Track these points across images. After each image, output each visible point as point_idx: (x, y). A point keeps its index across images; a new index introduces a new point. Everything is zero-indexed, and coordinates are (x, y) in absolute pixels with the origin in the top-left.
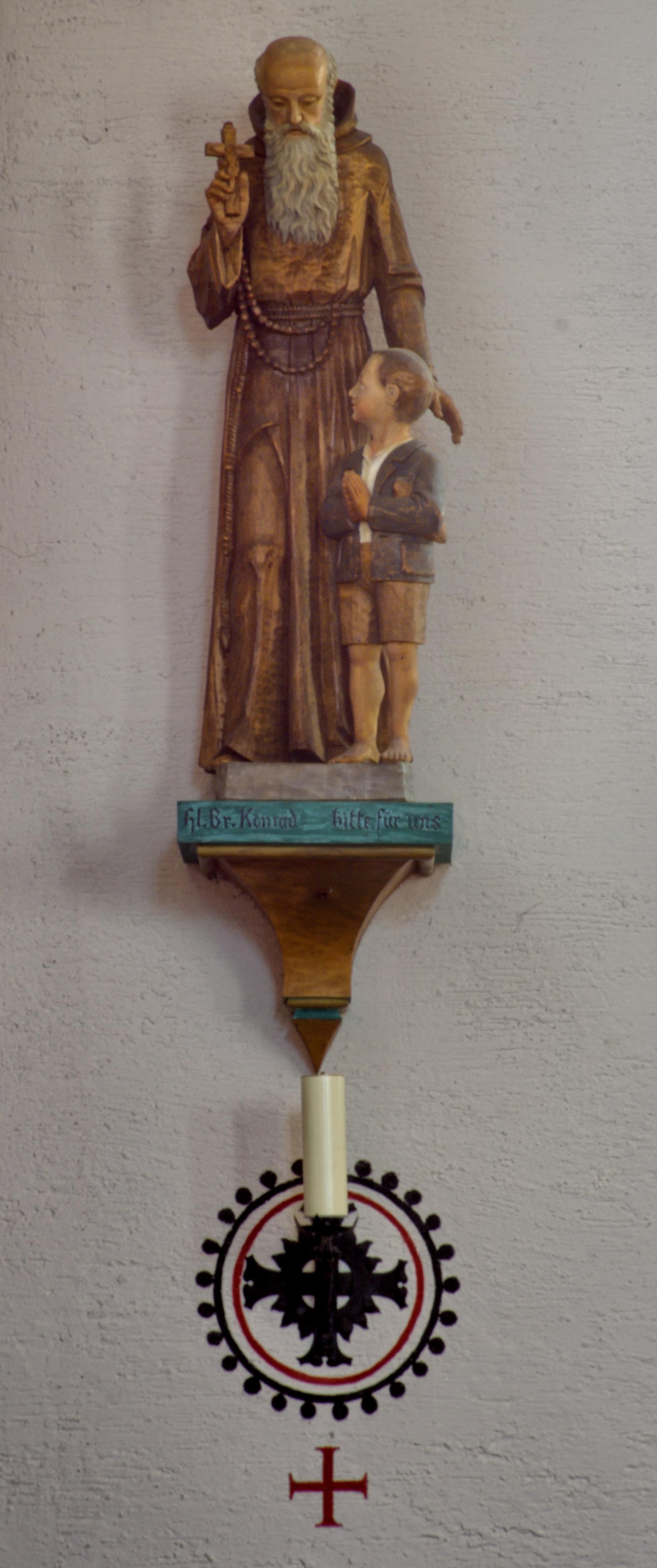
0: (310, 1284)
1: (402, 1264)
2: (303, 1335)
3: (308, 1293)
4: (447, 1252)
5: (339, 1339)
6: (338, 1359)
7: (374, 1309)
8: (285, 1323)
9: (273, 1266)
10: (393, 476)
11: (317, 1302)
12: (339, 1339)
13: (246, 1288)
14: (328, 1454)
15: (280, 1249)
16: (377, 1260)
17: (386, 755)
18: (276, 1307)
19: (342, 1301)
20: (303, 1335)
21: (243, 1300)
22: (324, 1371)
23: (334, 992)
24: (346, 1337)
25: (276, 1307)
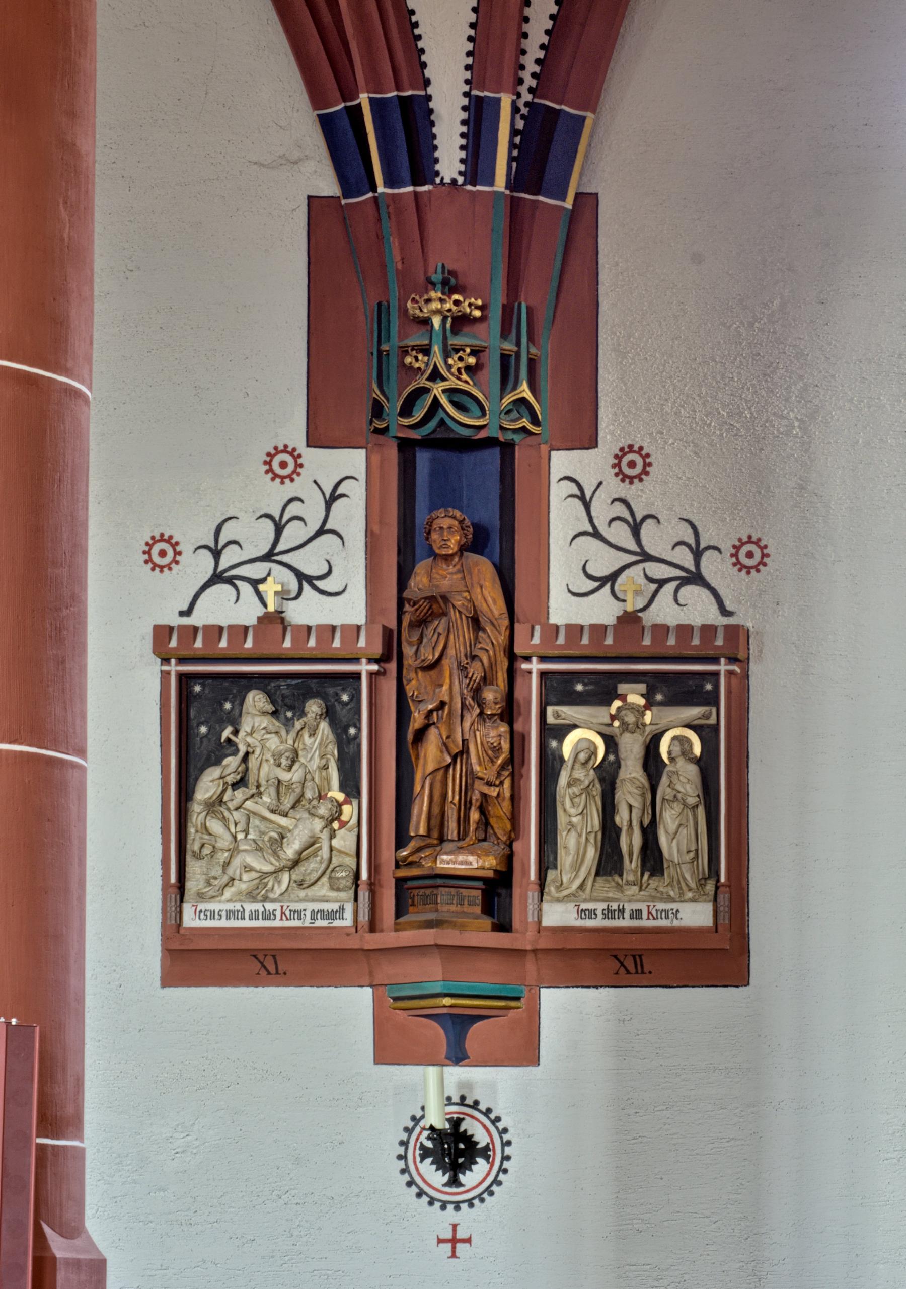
0: (460, 1153)
1: (422, 1161)
6: (423, 1158)
19: (461, 1160)
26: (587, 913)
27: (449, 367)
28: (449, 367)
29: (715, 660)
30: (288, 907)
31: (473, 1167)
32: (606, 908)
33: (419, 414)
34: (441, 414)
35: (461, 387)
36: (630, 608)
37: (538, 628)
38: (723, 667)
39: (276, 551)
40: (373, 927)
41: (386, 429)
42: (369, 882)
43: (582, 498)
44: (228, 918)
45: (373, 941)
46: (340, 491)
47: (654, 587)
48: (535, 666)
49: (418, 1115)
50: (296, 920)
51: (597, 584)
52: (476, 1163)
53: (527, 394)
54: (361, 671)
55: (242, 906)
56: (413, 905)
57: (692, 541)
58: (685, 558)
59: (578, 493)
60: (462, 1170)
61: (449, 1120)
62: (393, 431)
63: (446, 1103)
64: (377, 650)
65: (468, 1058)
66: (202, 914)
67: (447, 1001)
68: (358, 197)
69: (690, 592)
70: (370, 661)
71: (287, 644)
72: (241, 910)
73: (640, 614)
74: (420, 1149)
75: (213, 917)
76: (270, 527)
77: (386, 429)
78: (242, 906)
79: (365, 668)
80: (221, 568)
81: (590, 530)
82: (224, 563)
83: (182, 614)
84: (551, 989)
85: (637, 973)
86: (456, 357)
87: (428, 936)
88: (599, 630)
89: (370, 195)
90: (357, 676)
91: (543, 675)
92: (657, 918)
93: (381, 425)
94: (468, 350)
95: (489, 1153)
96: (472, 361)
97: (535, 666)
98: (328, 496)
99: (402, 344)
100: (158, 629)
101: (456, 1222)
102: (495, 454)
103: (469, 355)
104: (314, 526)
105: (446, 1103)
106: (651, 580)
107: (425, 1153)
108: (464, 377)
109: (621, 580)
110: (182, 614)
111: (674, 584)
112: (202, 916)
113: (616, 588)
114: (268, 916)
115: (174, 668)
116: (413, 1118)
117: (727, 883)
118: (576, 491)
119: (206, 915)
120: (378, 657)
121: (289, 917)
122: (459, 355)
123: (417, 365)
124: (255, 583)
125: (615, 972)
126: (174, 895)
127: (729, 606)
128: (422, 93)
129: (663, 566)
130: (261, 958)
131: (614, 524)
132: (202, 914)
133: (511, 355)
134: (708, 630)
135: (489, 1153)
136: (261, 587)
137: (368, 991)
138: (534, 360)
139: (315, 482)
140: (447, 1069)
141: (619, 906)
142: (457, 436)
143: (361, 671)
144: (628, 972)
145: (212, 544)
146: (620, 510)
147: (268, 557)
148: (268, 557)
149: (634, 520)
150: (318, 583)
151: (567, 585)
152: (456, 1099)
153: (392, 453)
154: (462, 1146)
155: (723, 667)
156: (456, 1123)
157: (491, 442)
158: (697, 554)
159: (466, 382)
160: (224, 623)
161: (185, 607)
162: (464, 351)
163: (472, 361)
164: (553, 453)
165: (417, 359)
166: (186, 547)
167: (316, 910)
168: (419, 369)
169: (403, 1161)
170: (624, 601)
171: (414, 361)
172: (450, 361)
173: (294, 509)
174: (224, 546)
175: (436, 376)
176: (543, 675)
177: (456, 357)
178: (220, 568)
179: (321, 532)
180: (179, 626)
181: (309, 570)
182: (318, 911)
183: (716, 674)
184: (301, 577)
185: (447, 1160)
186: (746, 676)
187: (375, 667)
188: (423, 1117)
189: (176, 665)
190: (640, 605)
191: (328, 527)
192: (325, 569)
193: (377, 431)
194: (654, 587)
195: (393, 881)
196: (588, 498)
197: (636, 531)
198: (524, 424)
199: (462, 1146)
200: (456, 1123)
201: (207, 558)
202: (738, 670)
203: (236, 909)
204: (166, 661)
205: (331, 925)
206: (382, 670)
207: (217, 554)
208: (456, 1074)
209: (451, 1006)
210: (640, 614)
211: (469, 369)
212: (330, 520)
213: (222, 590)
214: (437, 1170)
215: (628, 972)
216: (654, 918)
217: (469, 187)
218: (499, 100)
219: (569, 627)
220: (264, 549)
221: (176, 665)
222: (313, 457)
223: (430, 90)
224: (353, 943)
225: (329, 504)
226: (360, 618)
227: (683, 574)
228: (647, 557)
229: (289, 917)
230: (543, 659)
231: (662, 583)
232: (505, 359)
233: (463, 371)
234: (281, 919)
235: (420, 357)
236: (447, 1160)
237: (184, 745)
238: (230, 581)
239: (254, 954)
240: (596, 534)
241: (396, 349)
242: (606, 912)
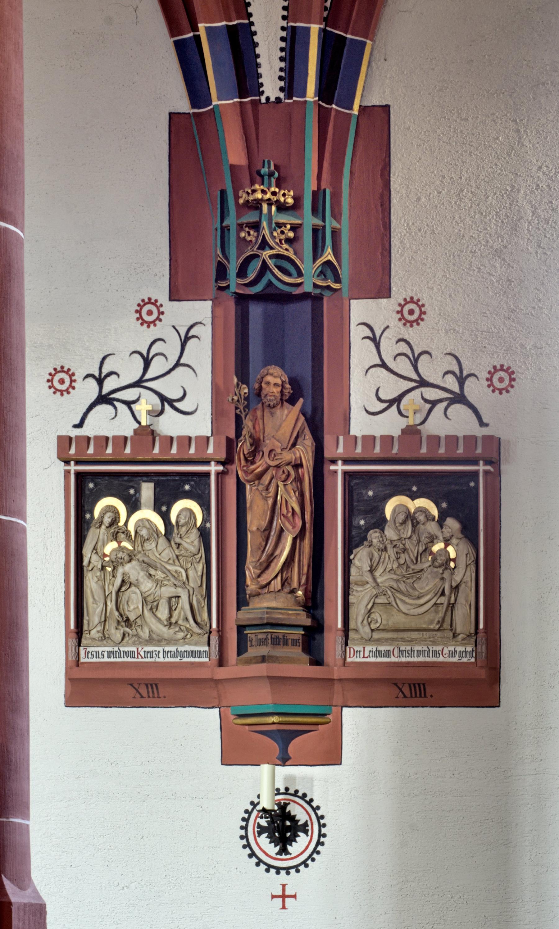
0: (289, 829)
1: (307, 821)
2: (289, 812)
13: (258, 831)
14: (284, 886)
16: (267, 837)
18: (267, 837)
19: (288, 834)
21: (257, 835)
22: (284, 857)
23: (300, 222)
25: (267, 837)
27: (274, 238)
28: (274, 238)
29: (475, 462)
31: (273, 844)
33: (251, 276)
34: (268, 276)
35: (282, 253)
36: (411, 423)
37: (341, 438)
38: (481, 468)
40: (221, 662)
41: (228, 287)
42: (217, 629)
43: (373, 339)
44: (109, 657)
45: (222, 673)
46: (190, 334)
47: (428, 406)
48: (340, 467)
49: (256, 801)
51: (385, 405)
52: (299, 836)
53: (331, 258)
54: (211, 471)
55: (119, 649)
56: (252, 646)
57: (457, 371)
58: (452, 383)
60: (288, 842)
61: (279, 804)
62: (233, 289)
63: (276, 792)
64: (223, 456)
66: (90, 654)
67: (275, 719)
68: (204, 108)
69: (458, 409)
70: (218, 463)
71: (156, 450)
72: (428, 650)
73: (419, 427)
74: (258, 828)
76: (140, 363)
77: (228, 287)
78: (119, 649)
79: (213, 468)
80: (105, 391)
83: (75, 426)
85: (412, 697)
86: (279, 231)
87: (262, 669)
88: (388, 440)
90: (207, 475)
91: (346, 474)
93: (224, 284)
94: (289, 227)
95: (307, 828)
96: (291, 235)
97: (340, 467)
99: (240, 221)
100: (60, 439)
102: (307, 306)
103: (289, 230)
104: (172, 362)
105: (276, 792)
106: (426, 401)
107: (261, 830)
108: (285, 246)
109: (404, 402)
110: (75, 426)
111: (445, 404)
112: (90, 656)
113: (402, 407)
114: (435, 653)
115: (73, 468)
116: (252, 803)
118: (369, 334)
120: (223, 460)
122: (282, 229)
123: (249, 238)
124: (129, 404)
125: (396, 696)
126: (73, 642)
127: (485, 420)
128: (247, 21)
130: (136, 686)
131: (399, 358)
132: (90, 654)
133: (319, 229)
134: (470, 440)
136: (135, 407)
138: (336, 232)
140: (277, 768)
142: (277, 292)
143: (211, 471)
144: (405, 696)
146: (403, 348)
147: (137, 384)
148: (137, 384)
150: (176, 404)
152: (283, 790)
153: (231, 305)
154: (288, 823)
155: (481, 468)
156: (283, 807)
157: (306, 296)
158: (462, 381)
159: (287, 250)
160: (110, 435)
161: (77, 422)
162: (286, 227)
163: (291, 235)
165: (249, 234)
166: (79, 376)
168: (251, 241)
169: (319, 815)
170: (407, 417)
171: (247, 235)
172: (275, 234)
175: (264, 245)
176: (346, 474)
177: (279, 231)
178: (105, 391)
179: (178, 364)
180: (77, 437)
181: (173, 394)
182: (184, 651)
183: (476, 473)
184: (163, 399)
185: (277, 834)
186: (498, 473)
187: (221, 468)
188: (258, 803)
190: (418, 421)
191: (182, 361)
192: (181, 394)
193: (221, 289)
194: (428, 406)
195: (236, 627)
198: (329, 284)
199: (288, 823)
200: (283, 807)
201: (93, 384)
202: (492, 470)
203: (115, 650)
204: (67, 462)
206: (226, 470)
207: (100, 382)
208: (282, 771)
209: (279, 723)
210: (419, 427)
211: (289, 241)
213: (104, 409)
215: (405, 696)
216: (142, 658)
217: (287, 101)
218: (309, 29)
219: (364, 437)
220: (136, 377)
222: (169, 307)
223: (252, 19)
224: (205, 674)
226: (207, 432)
228: (423, 383)
229: (143, 656)
230: (346, 462)
231: (434, 403)
232: (315, 231)
233: (283, 242)
235: (252, 232)
236: (277, 834)
237: (79, 525)
239: (131, 683)
240: (384, 365)
241: (235, 226)
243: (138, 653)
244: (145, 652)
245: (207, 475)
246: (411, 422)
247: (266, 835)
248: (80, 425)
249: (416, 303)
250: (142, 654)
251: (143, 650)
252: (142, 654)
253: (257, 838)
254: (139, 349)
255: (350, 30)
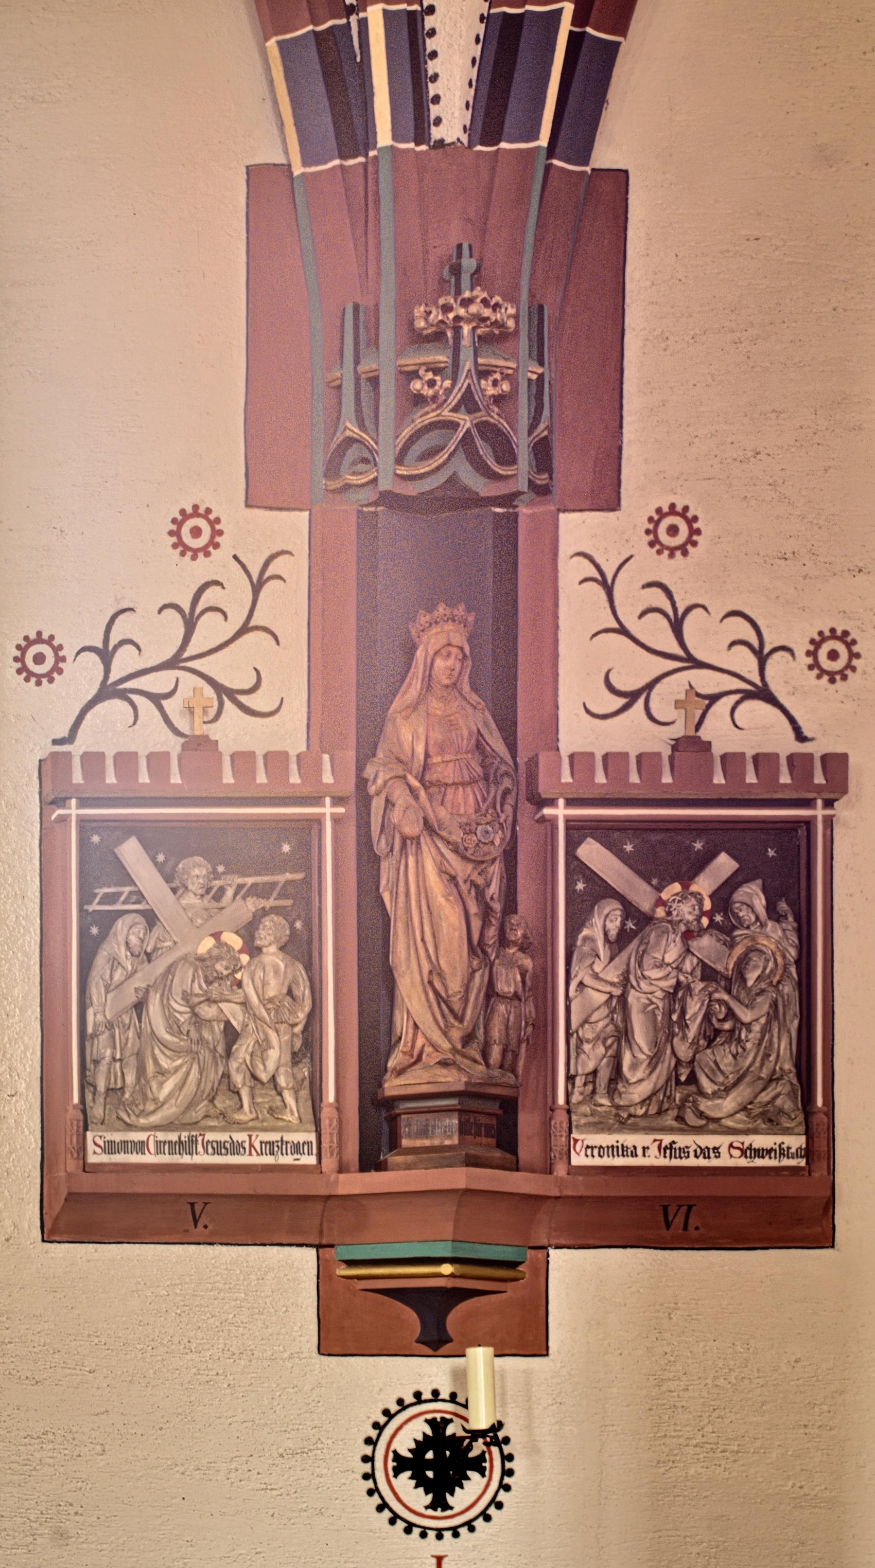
2: (427, 1493)
3: (429, 1470)
4: (418, 1395)
5: (448, 1495)
7: (468, 1478)
8: (417, 1486)
9: (410, 1455)
10: (253, 1098)
11: (434, 1475)
12: (448, 1495)
15: (413, 1446)
16: (425, 1434)
17: (464, 1050)
20: (427, 1493)
24: (452, 1494)
25: (411, 1478)
26: (215, 1145)
30: (257, 1136)
32: (279, 1139)
39: (186, 655)
42: (336, 1105)
50: (167, 1155)
55: (231, 1138)
59: (597, 575)
65: (449, 1340)
69: (757, 708)
70: (338, 801)
74: (394, 1460)
75: (634, 1154)
78: (231, 1138)
80: (114, 677)
81: (615, 625)
82: (119, 669)
84: (629, 1250)
89: (361, 159)
90: (318, 821)
92: (262, 1154)
95: (484, 1464)
98: (255, 579)
101: (441, 1554)
104: (236, 621)
114: (236, 1148)
117: (825, 1109)
119: (226, 1149)
121: (259, 1151)
124: (156, 699)
127: (807, 733)
129: (726, 677)
135: (484, 1464)
137: (313, 1252)
139: (235, 557)
141: (180, 1138)
145: (100, 645)
146: (658, 598)
147: (173, 663)
148: (173, 663)
149: (675, 610)
151: (584, 704)
158: (762, 659)
164: (562, 516)
167: (301, 1142)
173: (210, 597)
174: (116, 647)
178: (114, 677)
179: (245, 629)
182: (304, 1143)
189: (78, 808)
191: (253, 623)
196: (610, 581)
197: (677, 627)
205: (297, 1162)
207: (106, 655)
212: (256, 613)
213: (115, 707)
214: (416, 1487)
220: (169, 653)
221: (78, 808)
225: (257, 588)
227: (749, 687)
229: (259, 1151)
230: (571, 802)
231: (714, 698)
234: (250, 1154)
238: (123, 695)
240: (622, 631)
242: (280, 1144)
243: (251, 1145)
244: (261, 1143)
245: (318, 821)
246: (678, 731)
247: (408, 1473)
248: (70, 738)
249: (655, 532)
250: (257, 1145)
251: (260, 1139)
252: (257, 1145)
253: (393, 1480)
254: (88, 643)
255: (592, 20)
